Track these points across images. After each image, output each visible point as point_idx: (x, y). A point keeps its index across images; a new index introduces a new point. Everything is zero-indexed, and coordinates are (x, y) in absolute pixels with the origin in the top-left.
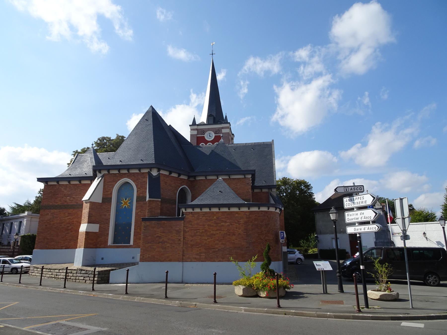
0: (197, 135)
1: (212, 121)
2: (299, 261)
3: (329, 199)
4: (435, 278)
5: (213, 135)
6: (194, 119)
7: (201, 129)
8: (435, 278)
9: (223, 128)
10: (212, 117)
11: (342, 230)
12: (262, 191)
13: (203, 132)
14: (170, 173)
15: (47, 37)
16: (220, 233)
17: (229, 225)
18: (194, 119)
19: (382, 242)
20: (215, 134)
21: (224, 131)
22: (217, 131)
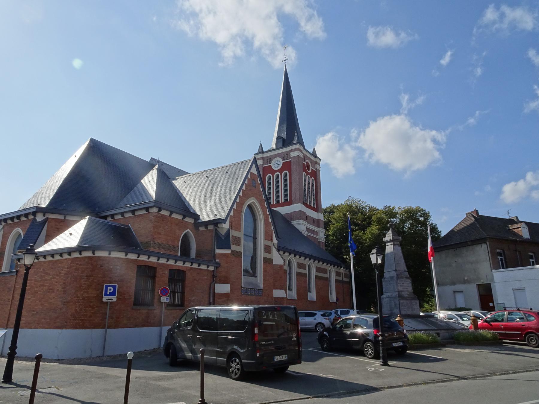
0: (263, 165)
1: (280, 144)
2: (320, 328)
3: (452, 231)
4: (238, 369)
5: (281, 162)
6: (261, 145)
7: (267, 157)
8: (238, 369)
9: (291, 151)
10: (281, 140)
11: (466, 278)
12: (207, 228)
13: (269, 160)
14: (184, 218)
15: (407, 97)
16: (42, 289)
17: (51, 279)
18: (261, 145)
19: (389, 297)
20: (283, 160)
21: (293, 154)
22: (285, 156)
